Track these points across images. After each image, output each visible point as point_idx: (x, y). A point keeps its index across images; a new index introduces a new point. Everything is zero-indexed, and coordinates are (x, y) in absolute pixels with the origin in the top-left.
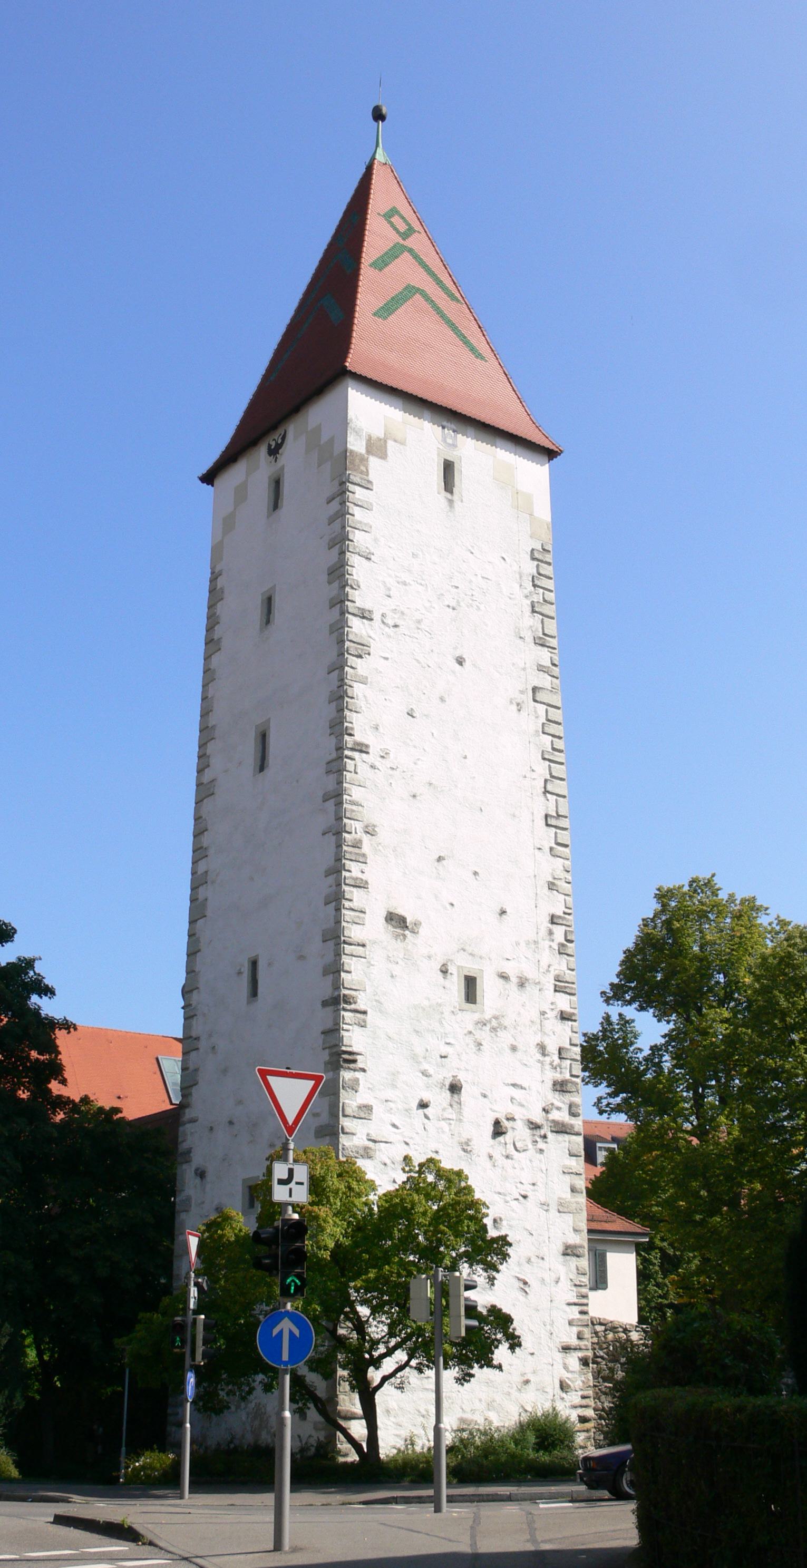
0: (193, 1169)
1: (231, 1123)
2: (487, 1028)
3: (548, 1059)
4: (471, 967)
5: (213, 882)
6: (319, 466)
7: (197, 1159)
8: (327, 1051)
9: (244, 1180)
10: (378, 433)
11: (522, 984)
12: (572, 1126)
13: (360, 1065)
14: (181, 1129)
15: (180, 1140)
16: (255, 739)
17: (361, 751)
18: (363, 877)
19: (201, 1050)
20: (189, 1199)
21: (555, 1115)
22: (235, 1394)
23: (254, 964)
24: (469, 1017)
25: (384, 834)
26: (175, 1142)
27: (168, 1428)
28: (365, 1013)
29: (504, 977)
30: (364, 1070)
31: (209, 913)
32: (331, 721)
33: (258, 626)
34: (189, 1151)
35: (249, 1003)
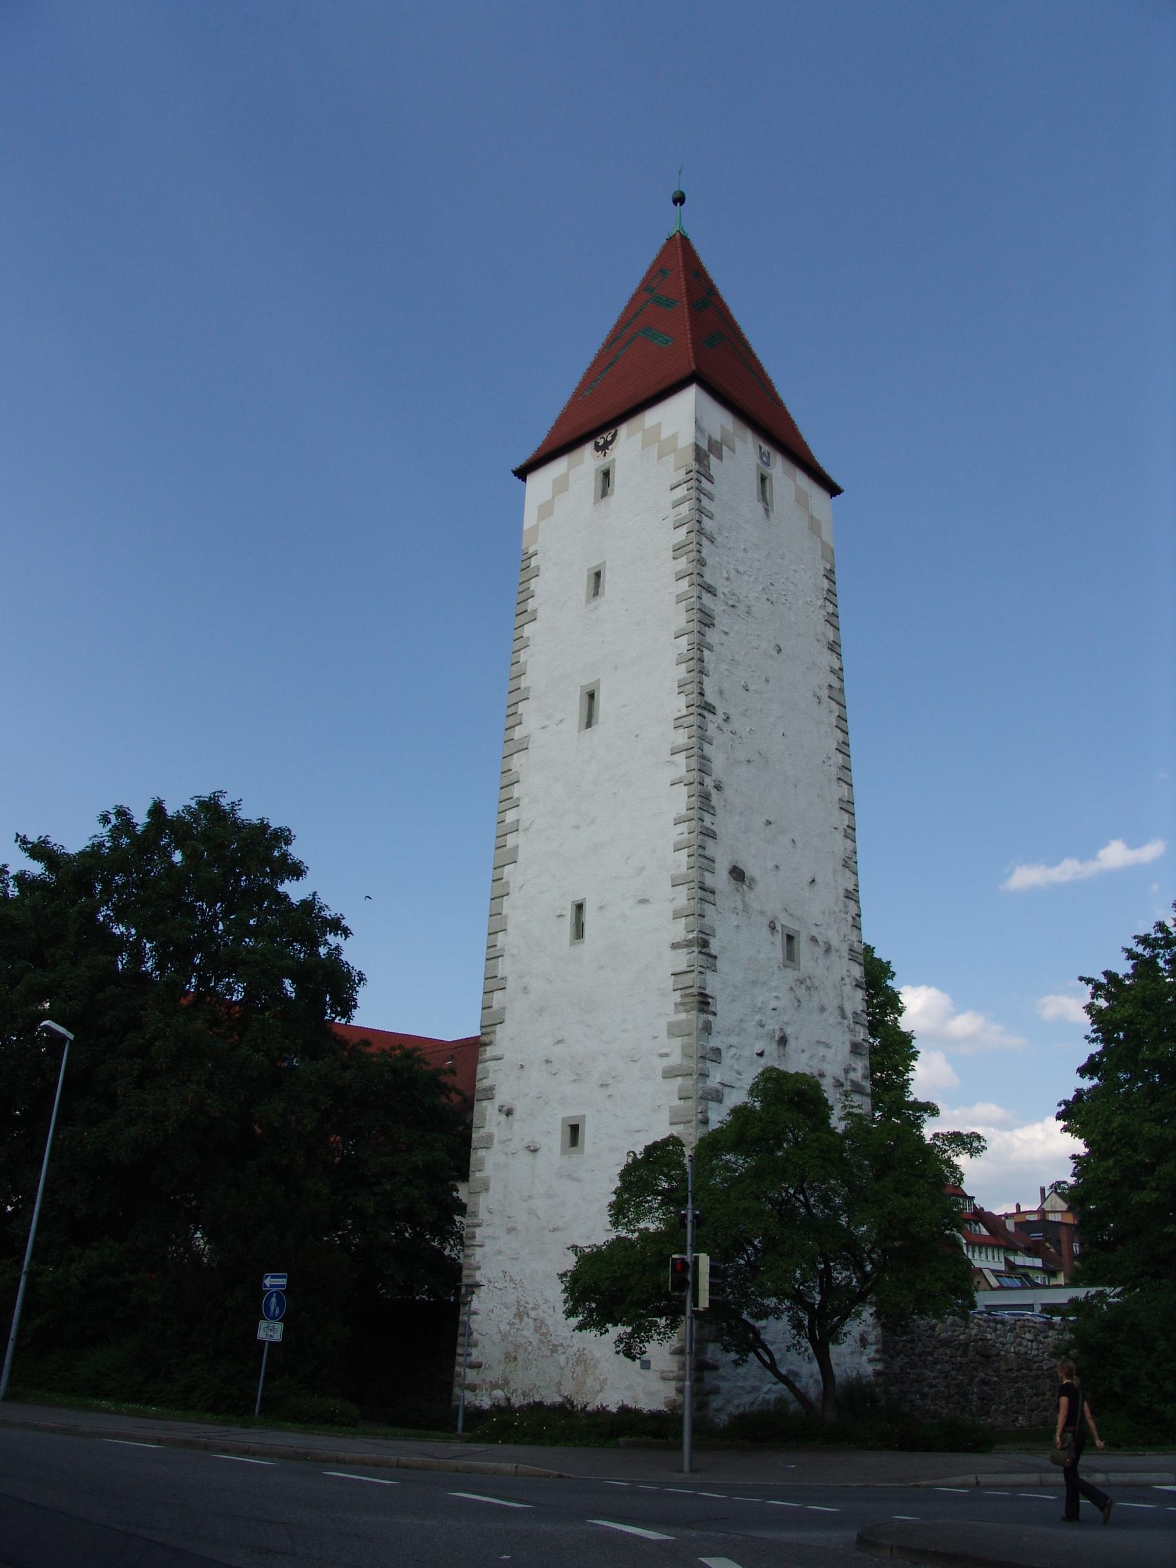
0: (497, 1107)
1: (548, 1061)
2: (803, 987)
3: (846, 1021)
4: (793, 925)
5: (527, 830)
6: (660, 458)
7: (502, 1097)
8: (679, 992)
9: (564, 1119)
10: (717, 436)
11: (828, 950)
12: (863, 1087)
13: (712, 1009)
14: (480, 1066)
15: (479, 1076)
16: (581, 699)
17: (709, 711)
18: (713, 828)
19: (508, 990)
20: (490, 1137)
21: (852, 1075)
22: (1021, 1388)
23: (579, 907)
24: (791, 975)
25: (728, 792)
26: (472, 1078)
27: (457, 1369)
28: (715, 957)
29: (814, 940)
30: (715, 1014)
31: (520, 859)
32: (679, 681)
33: (583, 598)
34: (491, 1089)
35: (572, 944)
